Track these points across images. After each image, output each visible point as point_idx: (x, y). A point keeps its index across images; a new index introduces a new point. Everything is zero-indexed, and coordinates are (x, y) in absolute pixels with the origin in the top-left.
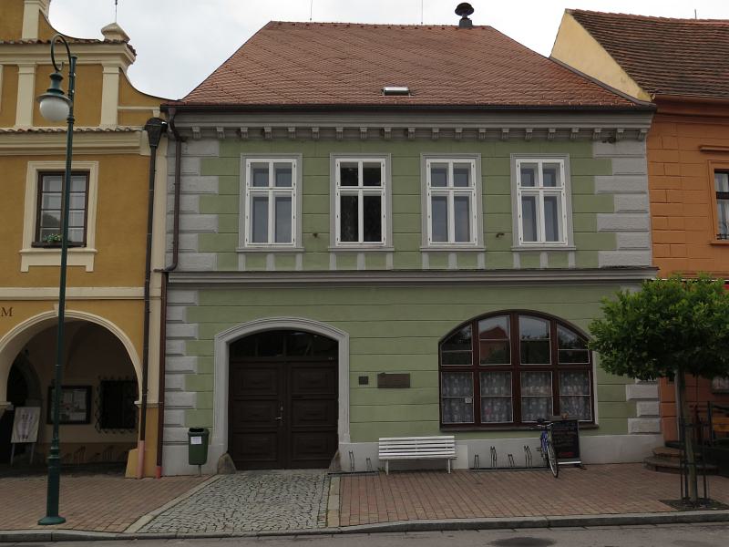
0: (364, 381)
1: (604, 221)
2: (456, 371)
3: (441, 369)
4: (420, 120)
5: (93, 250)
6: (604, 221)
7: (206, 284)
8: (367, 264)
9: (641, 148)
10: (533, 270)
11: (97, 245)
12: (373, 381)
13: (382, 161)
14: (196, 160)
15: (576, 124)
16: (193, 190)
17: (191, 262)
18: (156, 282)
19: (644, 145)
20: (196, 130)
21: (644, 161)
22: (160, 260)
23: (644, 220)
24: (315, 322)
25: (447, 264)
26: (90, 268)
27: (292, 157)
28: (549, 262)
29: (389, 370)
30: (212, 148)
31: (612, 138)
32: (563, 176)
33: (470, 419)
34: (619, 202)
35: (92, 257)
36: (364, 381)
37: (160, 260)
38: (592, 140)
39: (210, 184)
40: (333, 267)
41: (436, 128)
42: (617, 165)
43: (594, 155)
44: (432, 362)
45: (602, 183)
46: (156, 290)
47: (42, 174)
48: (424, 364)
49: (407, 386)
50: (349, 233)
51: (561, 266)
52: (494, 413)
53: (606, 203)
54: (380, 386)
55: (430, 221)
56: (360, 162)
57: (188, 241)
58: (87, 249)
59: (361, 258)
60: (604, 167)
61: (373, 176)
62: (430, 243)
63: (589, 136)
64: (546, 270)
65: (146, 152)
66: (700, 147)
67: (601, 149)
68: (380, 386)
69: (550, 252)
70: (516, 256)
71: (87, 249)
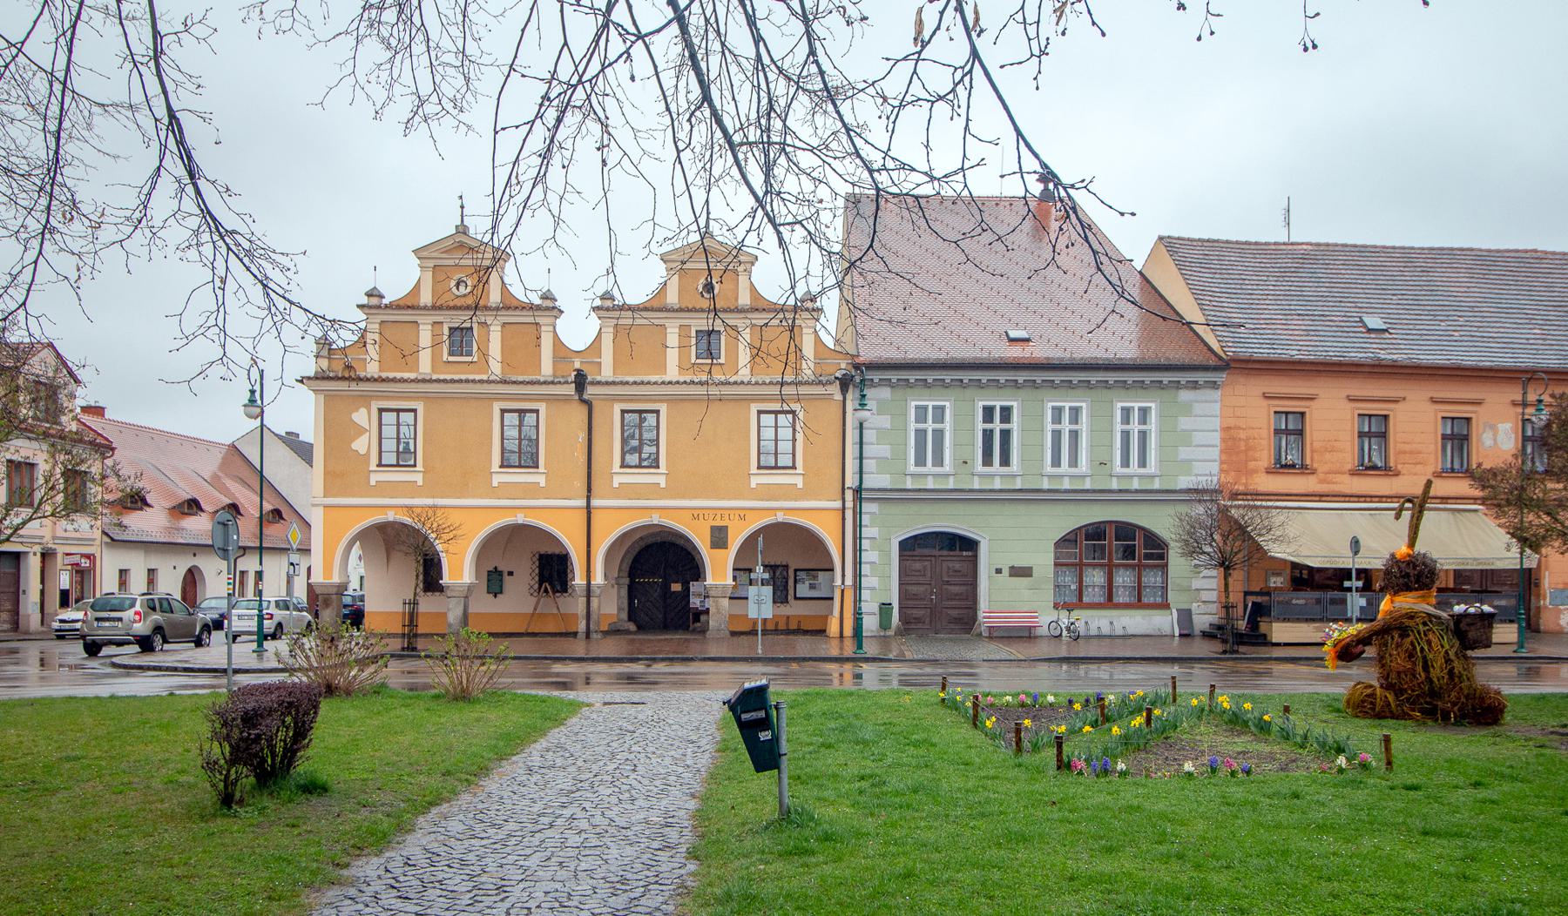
0: (999, 571)
1: (1184, 453)
2: (1482, 575)
3: (1056, 565)
4: (936, 373)
5: (422, 469)
6: (1184, 453)
7: (888, 497)
8: (1049, 484)
9: (1217, 394)
10: (1127, 491)
11: (805, 468)
12: (1006, 572)
13: (1014, 404)
14: (874, 402)
15: (1166, 377)
16: (872, 426)
17: (869, 482)
18: (849, 495)
19: (1219, 392)
20: (876, 381)
21: (1217, 406)
22: (851, 481)
23: (1215, 453)
24: (934, 524)
25: (1062, 485)
26: (800, 485)
27: (1152, 402)
28: (1139, 484)
29: (1017, 564)
30: (885, 393)
31: (1194, 386)
32: (1153, 416)
33: (1134, 600)
34: (1198, 438)
35: (544, 476)
36: (999, 571)
37: (851, 481)
38: (1178, 388)
39: (885, 421)
40: (976, 486)
41: (1002, 379)
42: (1198, 408)
43: (1179, 400)
44: (1049, 559)
45: (1185, 423)
46: (849, 504)
47: (503, 411)
48: (1043, 560)
49: (1030, 575)
50: (987, 460)
51: (1149, 487)
52: (1121, 597)
53: (1186, 438)
54: (1011, 575)
55: (1153, 452)
56: (998, 404)
57: (869, 464)
58: (797, 471)
59: (1066, 480)
60: (1187, 410)
61: (1006, 414)
62: (1049, 469)
63: (1177, 385)
64: (1137, 491)
65: (839, 397)
66: (1348, 396)
67: (1185, 395)
68: (1011, 575)
69: (1141, 477)
70: (1045, 479)
71: (797, 471)
